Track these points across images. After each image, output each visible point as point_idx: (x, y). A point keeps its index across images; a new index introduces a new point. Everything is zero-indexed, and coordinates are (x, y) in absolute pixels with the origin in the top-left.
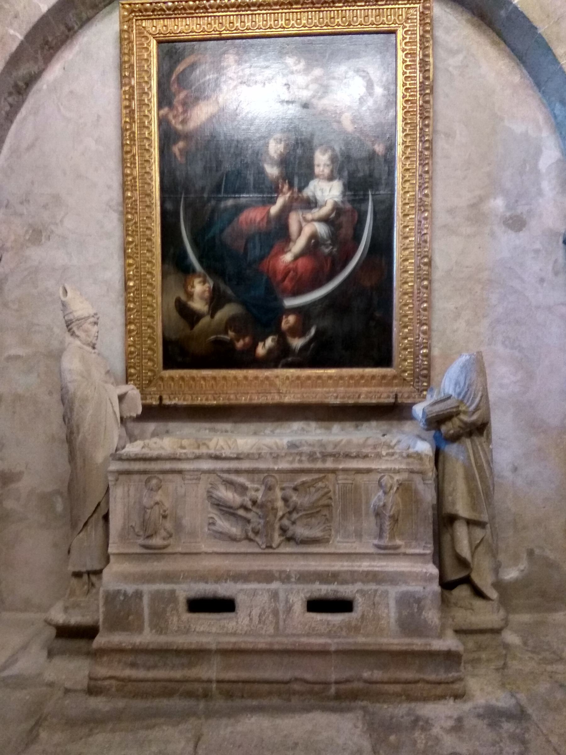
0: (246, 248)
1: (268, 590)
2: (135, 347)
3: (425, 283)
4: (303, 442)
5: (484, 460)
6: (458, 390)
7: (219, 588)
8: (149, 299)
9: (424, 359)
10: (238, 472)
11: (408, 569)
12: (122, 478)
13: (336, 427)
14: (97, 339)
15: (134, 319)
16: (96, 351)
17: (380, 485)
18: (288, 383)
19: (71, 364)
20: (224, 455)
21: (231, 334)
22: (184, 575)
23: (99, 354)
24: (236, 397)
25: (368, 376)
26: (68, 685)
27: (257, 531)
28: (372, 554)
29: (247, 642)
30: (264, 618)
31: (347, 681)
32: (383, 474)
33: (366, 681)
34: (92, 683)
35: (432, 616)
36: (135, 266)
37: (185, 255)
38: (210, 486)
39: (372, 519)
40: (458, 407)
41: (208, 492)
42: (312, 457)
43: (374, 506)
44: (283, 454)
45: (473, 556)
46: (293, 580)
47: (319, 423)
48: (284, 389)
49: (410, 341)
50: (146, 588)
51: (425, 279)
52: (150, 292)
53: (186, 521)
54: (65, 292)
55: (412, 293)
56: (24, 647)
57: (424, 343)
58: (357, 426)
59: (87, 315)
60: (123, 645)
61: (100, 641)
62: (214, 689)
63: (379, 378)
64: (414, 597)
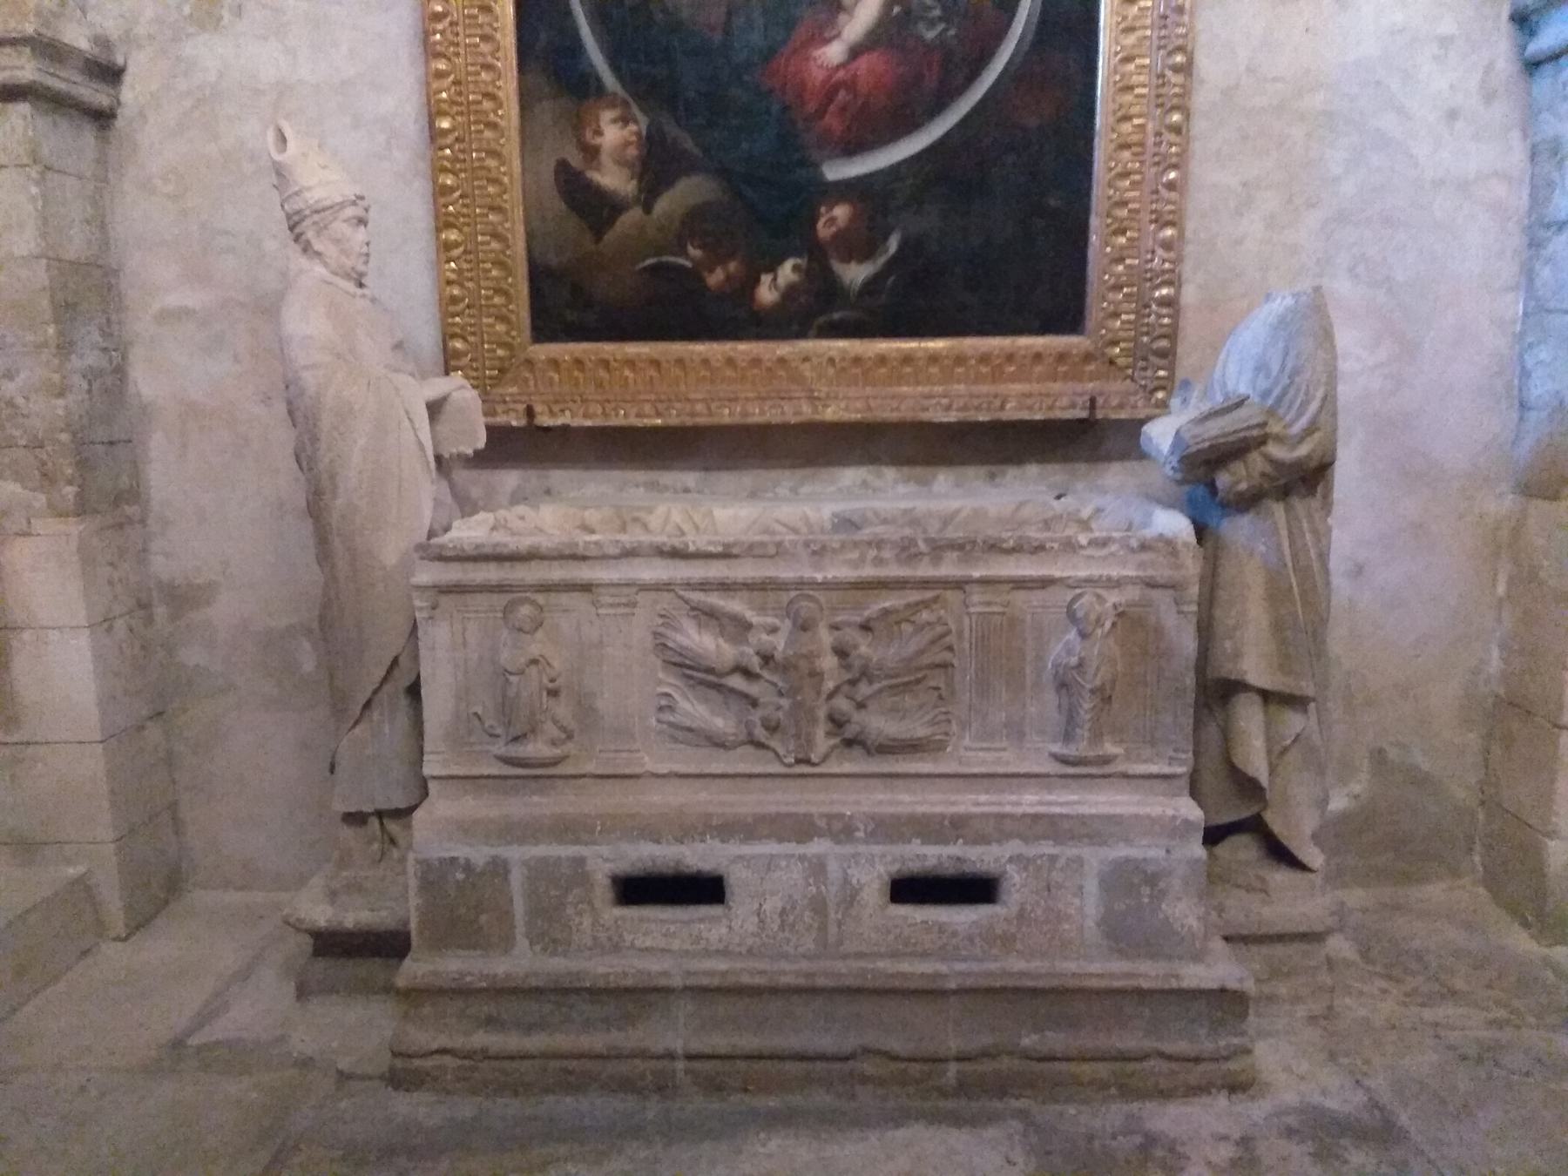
0: (727, 32)
1: (802, 858)
2: (462, 286)
3: (1176, 117)
4: (870, 514)
5: (1313, 554)
6: (1263, 384)
7: (688, 853)
8: (492, 163)
9: (1165, 311)
10: (725, 587)
11: (1133, 810)
12: (445, 600)
13: (943, 479)
14: (366, 263)
15: (457, 215)
16: (365, 291)
17: (1071, 615)
18: (832, 374)
19: (307, 325)
20: (692, 548)
21: (695, 252)
22: (603, 825)
23: (373, 300)
24: (709, 408)
25: (1024, 357)
26: (344, 1064)
27: (773, 724)
28: (1047, 776)
29: (749, 972)
30: (792, 918)
31: (985, 1054)
32: (1078, 591)
33: (1027, 1056)
34: (399, 1063)
35: (1184, 912)
36: (452, 77)
37: (575, 48)
38: (660, 621)
39: (1050, 697)
40: (1264, 425)
41: (656, 634)
42: (907, 552)
43: (1056, 666)
44: (836, 545)
45: (1272, 770)
46: (860, 834)
47: (906, 470)
48: (822, 390)
49: (1130, 267)
50: (515, 854)
51: (1174, 108)
52: (493, 145)
53: (605, 704)
54: (282, 139)
55: (1141, 144)
56: (244, 975)
57: (1164, 272)
58: (992, 476)
59: (339, 199)
60: (468, 979)
61: (415, 968)
62: (680, 1075)
63: (1051, 360)
64: (1145, 872)
